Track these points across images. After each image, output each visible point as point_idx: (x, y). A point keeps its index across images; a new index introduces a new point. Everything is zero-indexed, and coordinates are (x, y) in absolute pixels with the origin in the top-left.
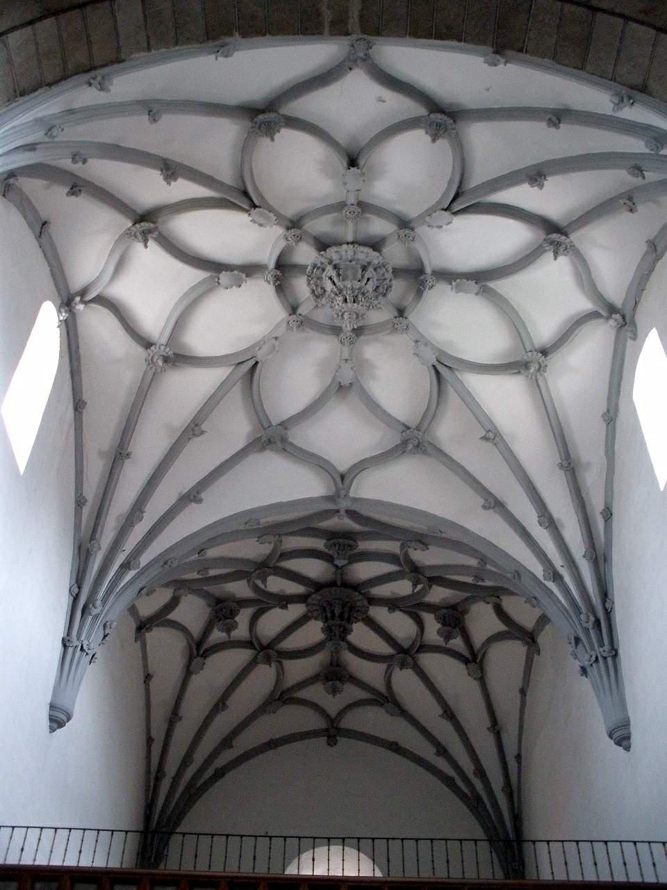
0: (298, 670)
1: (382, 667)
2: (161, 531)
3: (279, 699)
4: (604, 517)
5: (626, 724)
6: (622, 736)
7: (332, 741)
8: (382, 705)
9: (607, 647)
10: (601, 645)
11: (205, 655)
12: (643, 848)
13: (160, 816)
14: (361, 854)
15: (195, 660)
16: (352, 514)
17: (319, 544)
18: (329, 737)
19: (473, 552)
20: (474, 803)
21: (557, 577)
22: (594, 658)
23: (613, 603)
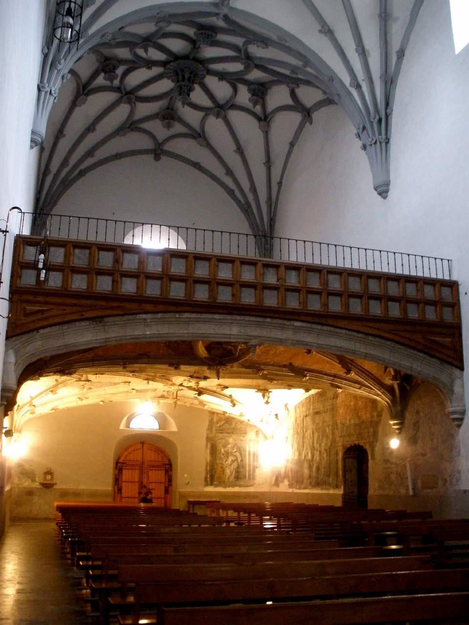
0: (144, 109)
1: (201, 114)
2: (103, 13)
3: (128, 128)
4: (398, 55)
5: (387, 184)
6: (383, 190)
7: (157, 157)
8: (195, 138)
9: (384, 136)
10: (380, 134)
11: (87, 95)
12: (425, 260)
13: (47, 194)
14: (52, 213)
15: (81, 97)
16: (226, 18)
17: (191, 32)
18: (156, 154)
19: (300, 55)
20: (246, 209)
21: (358, 87)
22: (374, 141)
23: (392, 111)
